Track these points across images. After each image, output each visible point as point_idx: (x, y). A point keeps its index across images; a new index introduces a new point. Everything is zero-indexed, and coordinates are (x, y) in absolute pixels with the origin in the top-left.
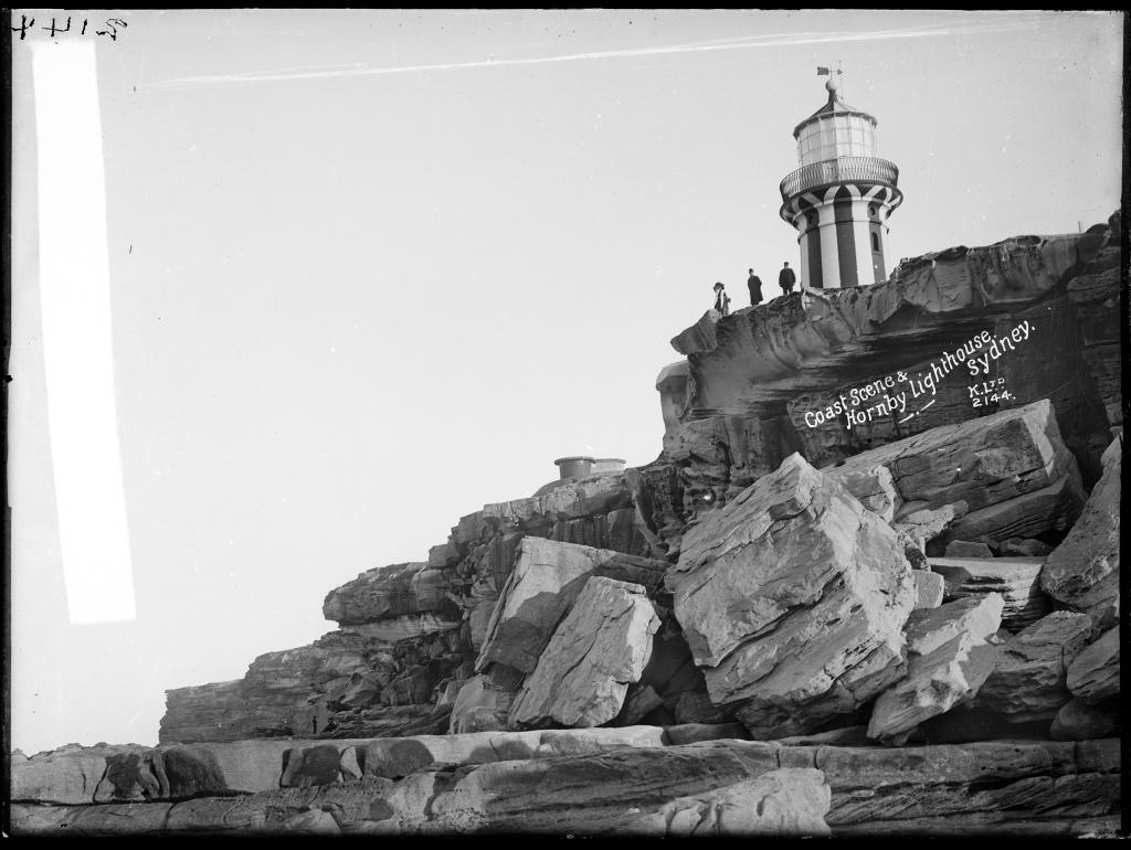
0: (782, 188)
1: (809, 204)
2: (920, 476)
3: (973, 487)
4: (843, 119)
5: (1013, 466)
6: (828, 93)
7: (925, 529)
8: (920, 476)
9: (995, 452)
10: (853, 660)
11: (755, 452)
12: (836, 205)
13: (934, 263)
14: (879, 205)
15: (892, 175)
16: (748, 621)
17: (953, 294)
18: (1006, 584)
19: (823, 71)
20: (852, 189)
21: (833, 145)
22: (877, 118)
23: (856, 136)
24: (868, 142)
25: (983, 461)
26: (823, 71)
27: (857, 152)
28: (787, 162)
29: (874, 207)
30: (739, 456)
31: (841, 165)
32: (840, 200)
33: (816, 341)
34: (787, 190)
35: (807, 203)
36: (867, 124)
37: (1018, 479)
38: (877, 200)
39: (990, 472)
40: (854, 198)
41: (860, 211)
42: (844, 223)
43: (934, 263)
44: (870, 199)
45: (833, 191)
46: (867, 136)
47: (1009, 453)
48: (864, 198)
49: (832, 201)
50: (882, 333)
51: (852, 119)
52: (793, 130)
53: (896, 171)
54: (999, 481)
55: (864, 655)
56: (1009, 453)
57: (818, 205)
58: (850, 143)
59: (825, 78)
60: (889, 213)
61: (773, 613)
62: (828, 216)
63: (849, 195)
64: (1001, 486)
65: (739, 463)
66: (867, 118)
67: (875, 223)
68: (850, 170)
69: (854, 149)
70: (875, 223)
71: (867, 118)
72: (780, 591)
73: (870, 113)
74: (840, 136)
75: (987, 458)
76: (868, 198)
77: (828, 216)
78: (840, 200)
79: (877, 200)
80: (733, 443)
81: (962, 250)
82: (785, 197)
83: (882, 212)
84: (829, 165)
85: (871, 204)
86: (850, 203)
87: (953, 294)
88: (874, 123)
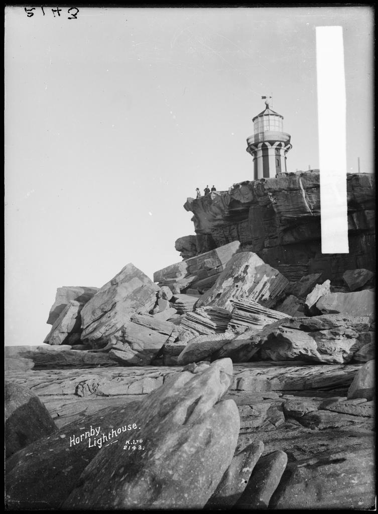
0: (248, 140)
1: (254, 149)
2: (194, 266)
3: (204, 271)
4: (267, 117)
5: (214, 264)
6: (266, 106)
7: (180, 285)
8: (194, 266)
9: (209, 260)
10: (107, 328)
11: (205, 247)
12: (262, 149)
13: (241, 186)
14: (280, 149)
15: (288, 138)
16: (94, 316)
17: (247, 196)
18: (184, 305)
19: (264, 98)
20: (267, 144)
21: (263, 127)
22: (284, 117)
23: (272, 123)
24: (281, 126)
25: (206, 263)
26: (264, 98)
27: (272, 129)
28: (249, 132)
29: (277, 150)
30: (199, 249)
31: (265, 134)
32: (264, 148)
33: (218, 210)
34: (249, 141)
35: (258, 148)
36: (281, 119)
37: (216, 268)
38: (278, 147)
39: (208, 266)
40: (268, 147)
41: (272, 152)
42: (266, 156)
43: (241, 186)
44: (276, 147)
45: (261, 145)
46: (280, 123)
47: (213, 260)
48: (273, 147)
49: (261, 148)
50: (232, 208)
51: (270, 116)
52: (252, 118)
53: (290, 137)
54: (210, 269)
55: (110, 327)
56: (213, 260)
57: (256, 150)
58: (269, 126)
59: (264, 100)
60: (286, 151)
61: (100, 314)
62: (260, 154)
63: (267, 146)
64: (211, 271)
65: (199, 251)
66: (281, 117)
67: (278, 155)
68: (269, 137)
69: (273, 129)
70: (278, 155)
71: (281, 117)
72: (102, 307)
73: (281, 115)
74: (265, 123)
75: (207, 262)
76: (275, 146)
77: (260, 154)
78: (264, 148)
79: (278, 147)
80: (197, 244)
81: (248, 182)
82: (248, 144)
83: (282, 152)
84: (262, 134)
85: (276, 149)
86: (267, 149)
87: (247, 196)
88: (283, 119)
